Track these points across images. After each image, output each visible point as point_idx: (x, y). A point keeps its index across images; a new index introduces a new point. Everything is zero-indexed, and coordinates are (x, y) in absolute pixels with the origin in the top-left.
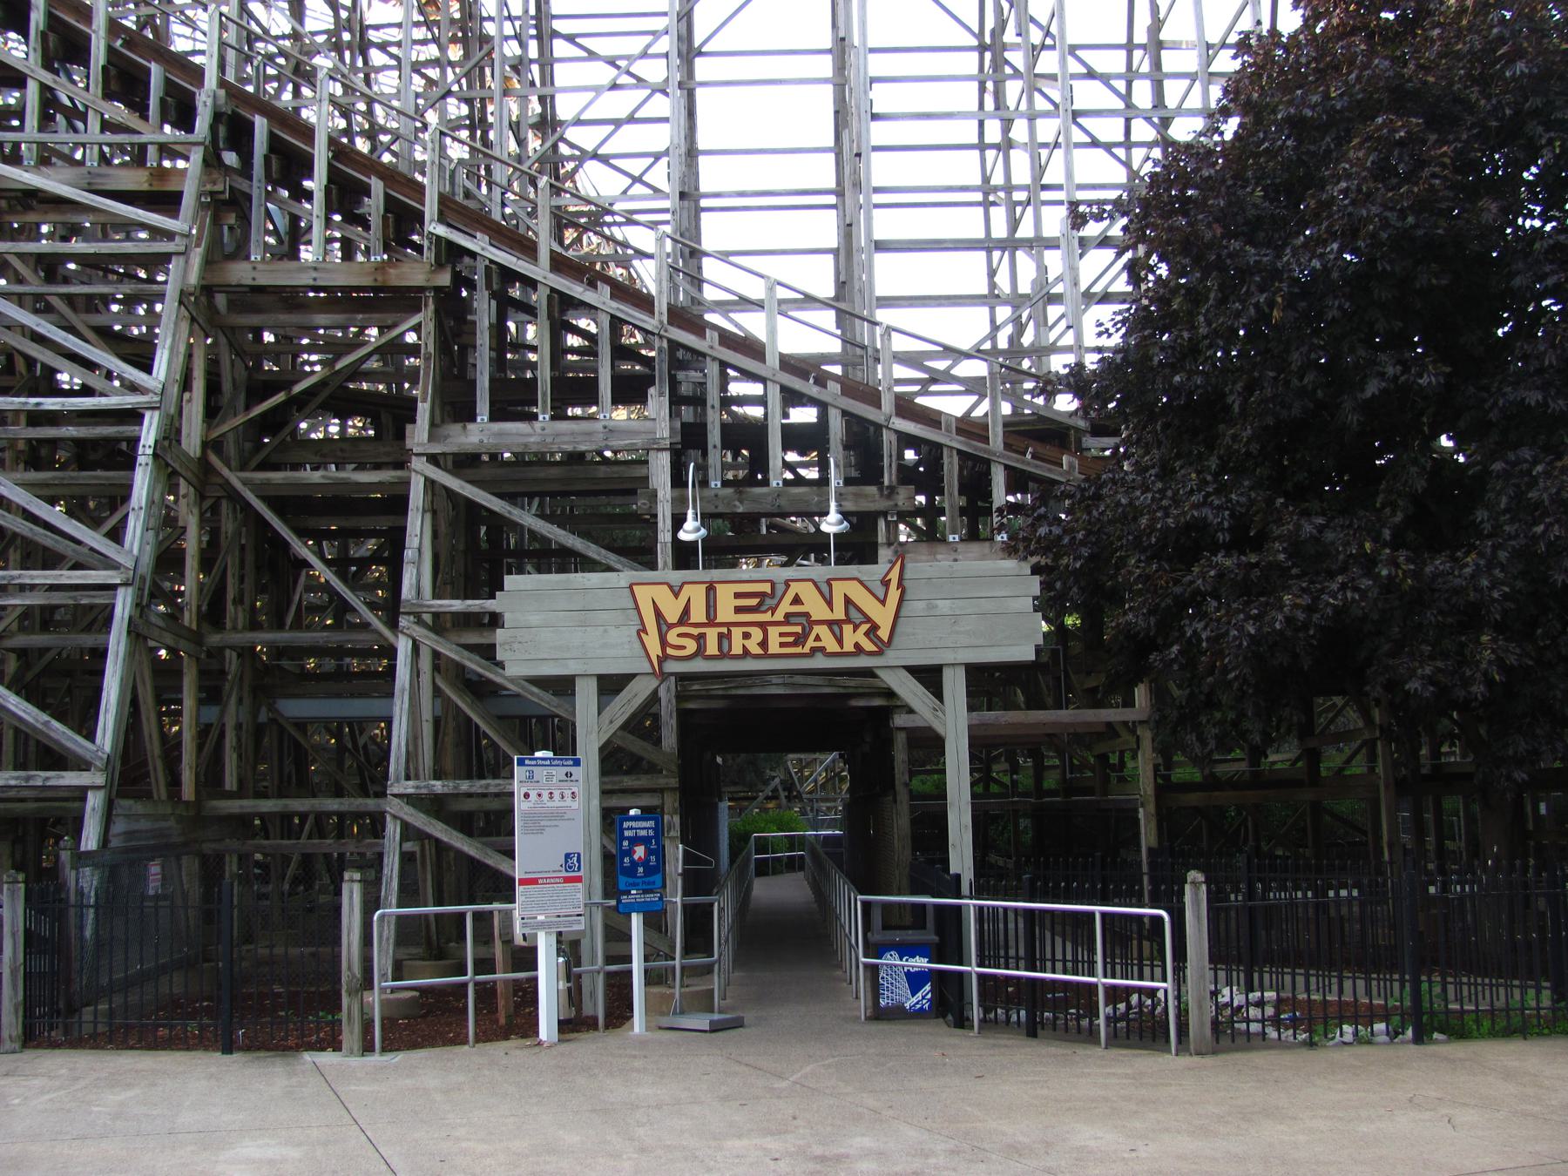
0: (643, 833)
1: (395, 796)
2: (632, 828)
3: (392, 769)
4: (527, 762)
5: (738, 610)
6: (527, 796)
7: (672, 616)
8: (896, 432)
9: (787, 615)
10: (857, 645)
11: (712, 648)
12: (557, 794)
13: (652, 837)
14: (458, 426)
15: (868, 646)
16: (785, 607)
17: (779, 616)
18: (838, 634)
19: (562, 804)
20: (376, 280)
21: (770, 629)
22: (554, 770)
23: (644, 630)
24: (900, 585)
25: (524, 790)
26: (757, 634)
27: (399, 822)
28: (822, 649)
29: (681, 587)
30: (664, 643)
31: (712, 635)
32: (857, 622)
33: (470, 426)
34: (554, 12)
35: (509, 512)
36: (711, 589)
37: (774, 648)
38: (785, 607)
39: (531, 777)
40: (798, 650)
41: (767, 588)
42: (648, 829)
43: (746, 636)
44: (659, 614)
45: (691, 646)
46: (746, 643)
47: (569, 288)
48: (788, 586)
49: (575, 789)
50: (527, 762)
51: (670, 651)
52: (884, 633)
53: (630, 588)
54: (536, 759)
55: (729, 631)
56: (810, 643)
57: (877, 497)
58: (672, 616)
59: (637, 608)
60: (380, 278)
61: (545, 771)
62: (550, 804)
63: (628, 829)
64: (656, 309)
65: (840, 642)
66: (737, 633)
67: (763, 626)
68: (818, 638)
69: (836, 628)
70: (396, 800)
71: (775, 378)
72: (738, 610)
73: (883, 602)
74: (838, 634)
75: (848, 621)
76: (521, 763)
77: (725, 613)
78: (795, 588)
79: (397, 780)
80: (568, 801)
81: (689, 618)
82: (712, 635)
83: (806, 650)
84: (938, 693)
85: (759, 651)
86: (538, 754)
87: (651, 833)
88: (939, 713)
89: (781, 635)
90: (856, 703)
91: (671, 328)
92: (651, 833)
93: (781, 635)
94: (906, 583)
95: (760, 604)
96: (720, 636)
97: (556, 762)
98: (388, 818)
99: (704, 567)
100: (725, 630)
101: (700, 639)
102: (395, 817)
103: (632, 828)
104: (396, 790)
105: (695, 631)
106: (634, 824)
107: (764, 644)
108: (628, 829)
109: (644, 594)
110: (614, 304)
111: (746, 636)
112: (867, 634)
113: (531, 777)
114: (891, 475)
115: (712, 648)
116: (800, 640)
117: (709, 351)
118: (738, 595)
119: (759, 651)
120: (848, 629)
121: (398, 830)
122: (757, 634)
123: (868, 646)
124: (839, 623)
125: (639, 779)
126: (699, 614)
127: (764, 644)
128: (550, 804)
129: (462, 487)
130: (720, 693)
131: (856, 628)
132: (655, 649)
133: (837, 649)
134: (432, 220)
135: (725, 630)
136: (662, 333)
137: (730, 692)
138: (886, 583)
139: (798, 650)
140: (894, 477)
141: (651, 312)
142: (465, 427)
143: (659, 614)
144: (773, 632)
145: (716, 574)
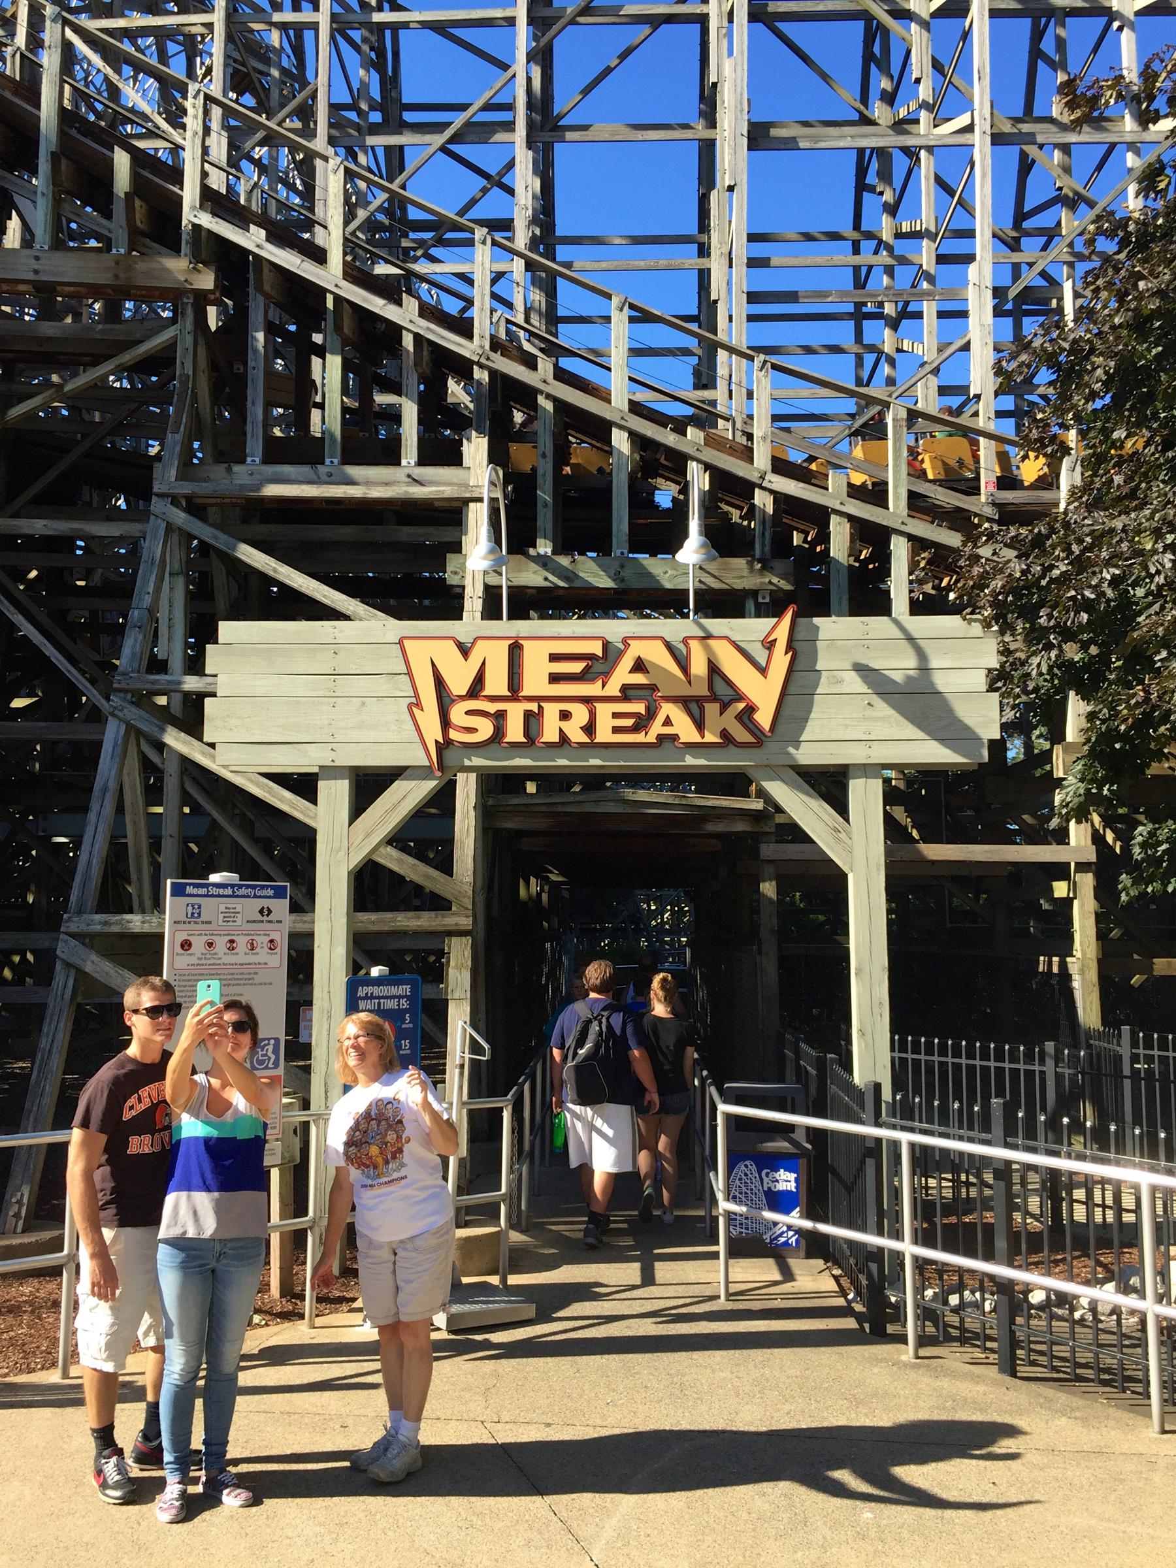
0: (391, 1004)
1: (73, 935)
2: (372, 997)
3: (73, 898)
4: (189, 890)
5: (555, 678)
6: (186, 945)
7: (458, 684)
8: (771, 491)
9: (625, 688)
10: (725, 734)
11: (515, 732)
12: (242, 943)
13: (405, 1011)
14: (222, 467)
15: (741, 734)
16: (622, 675)
17: (613, 688)
18: (697, 715)
19: (252, 958)
20: (116, 277)
21: (599, 706)
22: (238, 904)
23: (419, 705)
24: (790, 647)
25: (181, 936)
26: (580, 714)
27: (73, 972)
28: (674, 738)
29: (473, 644)
30: (446, 723)
31: (515, 714)
32: (726, 699)
33: (237, 468)
34: (406, 100)
35: (275, 570)
36: (515, 650)
37: (604, 734)
38: (622, 675)
39: (195, 914)
40: (639, 738)
41: (596, 648)
42: (400, 997)
43: (565, 716)
44: (439, 682)
45: (485, 729)
46: (565, 726)
47: (366, 300)
48: (627, 646)
49: (275, 936)
50: (189, 890)
51: (454, 735)
52: (764, 718)
53: (400, 643)
54: (207, 886)
55: (540, 708)
56: (657, 728)
57: (746, 573)
58: (458, 684)
59: (409, 673)
60: (122, 275)
61: (222, 905)
62: (230, 959)
63: (366, 998)
64: (476, 332)
65: (700, 726)
66: (551, 711)
67: (587, 700)
68: (668, 722)
69: (694, 707)
70: (73, 942)
71: (623, 423)
72: (555, 678)
73: (763, 671)
74: (697, 715)
75: (714, 698)
76: (178, 891)
77: (535, 681)
78: (637, 649)
79: (80, 912)
80: (263, 955)
81: (482, 688)
82: (515, 714)
83: (651, 738)
84: (842, 808)
85: (585, 739)
86: (215, 878)
87: (405, 1004)
88: (843, 836)
89: (616, 715)
90: (712, 827)
91: (493, 355)
92: (405, 1004)
93: (616, 715)
94: (796, 645)
95: (587, 670)
96: (528, 715)
97: (243, 891)
98: (59, 966)
99: (510, 618)
100: (533, 707)
101: (500, 716)
102: (68, 965)
103: (372, 997)
104: (73, 928)
105: (492, 708)
106: (376, 990)
107: (589, 729)
108: (366, 998)
109: (420, 654)
110: (423, 323)
111: (565, 716)
112: (739, 717)
113: (195, 914)
114: (763, 545)
115: (515, 732)
116: (641, 723)
117: (541, 386)
118: (554, 658)
119: (585, 739)
120: (712, 709)
121: (71, 983)
122: (580, 714)
123: (741, 734)
124: (700, 701)
125: (419, 918)
126: (497, 683)
127: (589, 729)
128: (230, 959)
129: (215, 538)
130: (543, 809)
131: (724, 707)
132: (433, 732)
133: (695, 737)
134: (193, 208)
135: (533, 707)
136: (483, 361)
137: (554, 809)
138: (770, 645)
139: (639, 738)
140: (767, 549)
141: (469, 336)
142: (229, 470)
143: (439, 682)
144: (604, 712)
145: (521, 627)
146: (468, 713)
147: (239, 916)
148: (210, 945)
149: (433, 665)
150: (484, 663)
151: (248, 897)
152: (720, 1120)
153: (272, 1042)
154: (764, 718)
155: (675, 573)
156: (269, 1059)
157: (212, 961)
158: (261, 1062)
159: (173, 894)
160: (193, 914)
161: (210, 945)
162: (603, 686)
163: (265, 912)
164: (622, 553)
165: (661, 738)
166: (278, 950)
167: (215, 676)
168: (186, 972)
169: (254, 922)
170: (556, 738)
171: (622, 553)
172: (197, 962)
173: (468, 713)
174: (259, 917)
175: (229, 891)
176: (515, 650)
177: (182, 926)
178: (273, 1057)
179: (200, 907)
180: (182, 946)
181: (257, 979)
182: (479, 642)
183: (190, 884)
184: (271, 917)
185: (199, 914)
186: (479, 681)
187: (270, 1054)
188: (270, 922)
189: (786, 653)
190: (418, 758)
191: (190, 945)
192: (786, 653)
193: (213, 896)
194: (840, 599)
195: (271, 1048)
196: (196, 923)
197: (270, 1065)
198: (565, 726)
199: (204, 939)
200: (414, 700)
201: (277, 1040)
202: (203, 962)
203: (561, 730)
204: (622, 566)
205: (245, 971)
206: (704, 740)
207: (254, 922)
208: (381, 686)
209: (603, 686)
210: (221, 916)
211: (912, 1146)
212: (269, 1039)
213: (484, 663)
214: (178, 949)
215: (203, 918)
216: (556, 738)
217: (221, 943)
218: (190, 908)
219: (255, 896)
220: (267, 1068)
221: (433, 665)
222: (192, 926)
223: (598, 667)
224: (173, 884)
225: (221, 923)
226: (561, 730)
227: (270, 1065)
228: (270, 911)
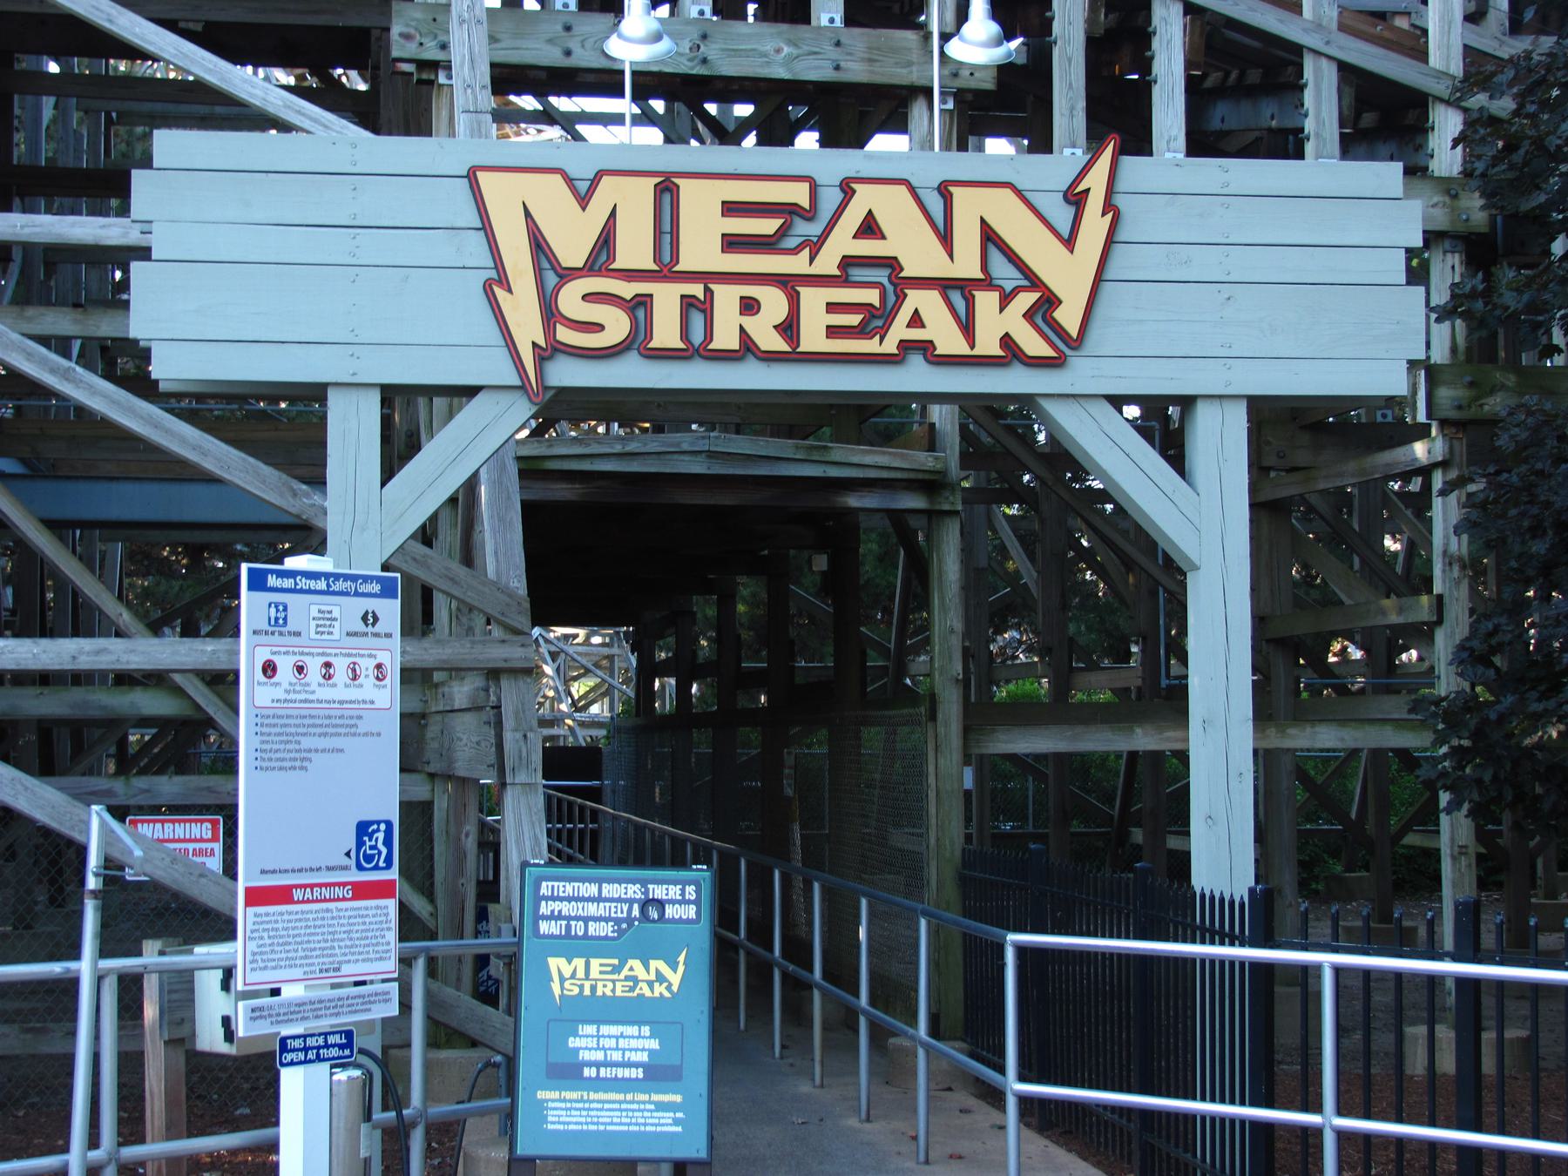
6: (269, 669)
7: (572, 248)
9: (847, 262)
10: (1007, 341)
11: (666, 333)
12: (341, 666)
15: (1034, 344)
19: (353, 694)
21: (806, 293)
23: (503, 281)
24: (1109, 206)
25: (263, 655)
26: (774, 303)
32: (1008, 286)
37: (813, 338)
38: (843, 242)
39: (279, 621)
41: (798, 194)
43: (749, 306)
44: (539, 246)
45: (617, 326)
46: (750, 323)
49: (384, 657)
50: (272, 581)
53: (471, 176)
55: (709, 293)
58: (572, 248)
59: (486, 227)
69: (957, 298)
73: (1069, 242)
76: (257, 582)
81: (612, 257)
89: (832, 307)
93: (832, 307)
94: (1119, 200)
95: (783, 232)
100: (697, 290)
101: (640, 306)
107: (789, 328)
113: (279, 621)
115: (666, 333)
118: (731, 209)
119: (780, 345)
122: (774, 303)
123: (1034, 344)
124: (965, 287)
126: (635, 249)
127: (789, 328)
131: (1006, 299)
132: (528, 328)
135: (697, 290)
143: (539, 246)
146: (586, 297)
147: (337, 624)
148: (300, 669)
149: (527, 214)
150: (613, 214)
151: (347, 594)
152: (1010, 956)
153: (383, 827)
154: (1069, 317)
155: (795, 52)
156: (380, 853)
157: (303, 696)
158: (369, 859)
159: (251, 588)
160: (277, 619)
161: (300, 669)
162: (811, 261)
163: (370, 618)
164: (702, 13)
165: (906, 346)
166: (387, 681)
167: (151, 222)
168: (271, 712)
169: (355, 634)
170: (734, 343)
171: (702, 13)
172: (283, 696)
173: (586, 297)
174: (361, 627)
175: (322, 585)
176: (667, 189)
177: (263, 639)
178: (384, 851)
179: (285, 609)
180: (265, 671)
181: (361, 730)
182: (605, 178)
183: (272, 572)
184: (378, 628)
185: (285, 619)
186: (606, 241)
187: (380, 845)
188: (376, 635)
189: (1103, 214)
190: (494, 368)
191: (274, 670)
192: (1103, 214)
193: (302, 591)
194: (1072, 109)
195: (381, 836)
196: (281, 634)
197: (381, 864)
198: (750, 323)
199: (292, 659)
200: (493, 274)
201: (389, 824)
202: (292, 696)
203: (741, 328)
204: (704, 37)
205: (347, 713)
206: (975, 352)
207: (355, 634)
208: (440, 249)
209: (811, 261)
210: (313, 624)
211: (1338, 971)
212: (378, 823)
213: (613, 214)
214: (259, 675)
215: (291, 626)
216: (734, 343)
217: (314, 666)
218: (273, 610)
219: (357, 594)
220: (376, 868)
221: (527, 214)
222: (276, 639)
223: (804, 229)
224: (250, 570)
225: (313, 635)
226: (741, 328)
227: (381, 864)
228: (376, 619)
